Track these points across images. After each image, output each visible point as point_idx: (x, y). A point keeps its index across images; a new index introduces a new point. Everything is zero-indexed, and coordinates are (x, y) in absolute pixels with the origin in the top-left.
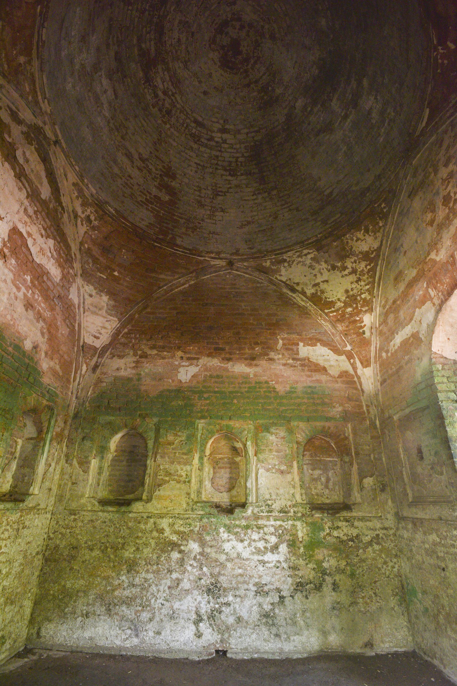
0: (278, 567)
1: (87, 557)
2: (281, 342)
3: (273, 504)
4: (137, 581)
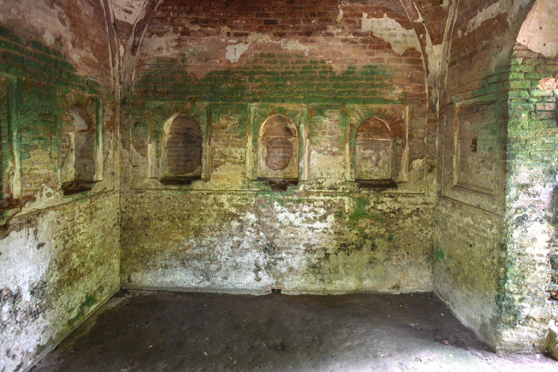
0: (325, 233)
1: (159, 226)
2: (341, 12)
3: (323, 182)
4: (204, 242)
